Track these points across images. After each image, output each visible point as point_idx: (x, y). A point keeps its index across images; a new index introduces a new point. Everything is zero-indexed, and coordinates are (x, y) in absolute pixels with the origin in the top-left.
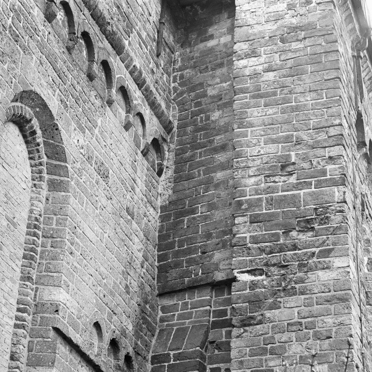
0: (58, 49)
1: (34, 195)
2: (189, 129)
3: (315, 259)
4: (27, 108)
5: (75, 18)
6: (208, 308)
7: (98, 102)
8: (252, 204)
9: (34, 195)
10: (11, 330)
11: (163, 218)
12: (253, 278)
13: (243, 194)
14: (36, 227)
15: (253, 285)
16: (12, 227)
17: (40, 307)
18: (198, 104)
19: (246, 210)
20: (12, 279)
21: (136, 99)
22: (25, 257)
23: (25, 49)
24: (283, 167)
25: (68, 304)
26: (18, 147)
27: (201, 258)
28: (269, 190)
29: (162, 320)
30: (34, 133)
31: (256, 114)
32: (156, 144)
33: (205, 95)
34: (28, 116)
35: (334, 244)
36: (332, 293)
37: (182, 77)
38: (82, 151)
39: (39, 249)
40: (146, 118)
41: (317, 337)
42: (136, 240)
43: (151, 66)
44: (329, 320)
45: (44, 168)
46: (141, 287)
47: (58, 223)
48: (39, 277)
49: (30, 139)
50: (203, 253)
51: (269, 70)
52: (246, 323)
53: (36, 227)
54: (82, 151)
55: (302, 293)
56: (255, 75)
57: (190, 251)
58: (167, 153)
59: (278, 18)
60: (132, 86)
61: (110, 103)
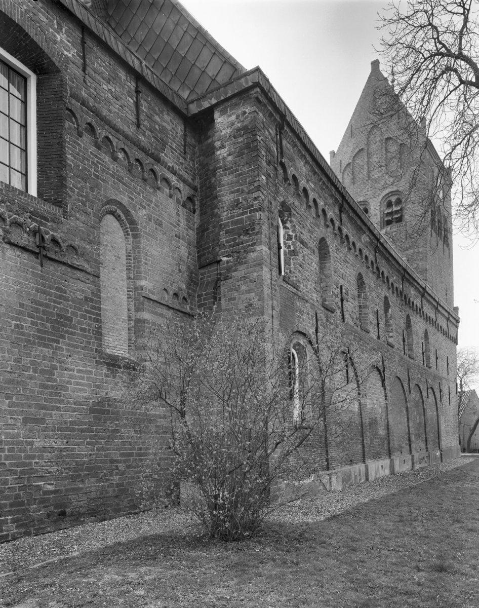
0: (123, 173)
1: (127, 242)
2: (204, 188)
3: (250, 248)
4: (113, 206)
5: (129, 154)
6: (216, 272)
7: (151, 190)
8: (227, 225)
9: (127, 242)
10: (126, 300)
11: (197, 234)
12: (228, 259)
13: (222, 220)
14: (129, 256)
15: (228, 262)
16: (118, 259)
17: (136, 289)
18: (207, 175)
19: (224, 228)
20: (122, 280)
21: (173, 181)
22: (127, 270)
23: (103, 180)
24: (237, 205)
25: (147, 285)
26: (114, 224)
27: (211, 250)
28: (232, 217)
29: (201, 279)
30: (119, 216)
31: (225, 179)
32: (190, 199)
33: (208, 170)
34: (114, 210)
35: (257, 240)
36: (256, 262)
37: (199, 161)
38: (145, 217)
39: (133, 265)
40: (181, 189)
41: (251, 281)
42: (183, 248)
43: (181, 161)
44: (255, 274)
45: (129, 230)
46: (189, 268)
47: (138, 253)
48: (134, 277)
49: (118, 219)
50: (213, 248)
51: (229, 155)
52: (226, 279)
53: (129, 256)
54: (145, 217)
55: (245, 264)
56: (224, 158)
57: (208, 248)
58: (196, 202)
59: (233, 124)
60: (169, 175)
61: (159, 189)
